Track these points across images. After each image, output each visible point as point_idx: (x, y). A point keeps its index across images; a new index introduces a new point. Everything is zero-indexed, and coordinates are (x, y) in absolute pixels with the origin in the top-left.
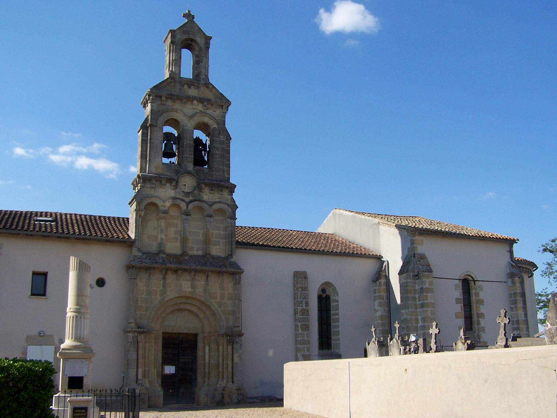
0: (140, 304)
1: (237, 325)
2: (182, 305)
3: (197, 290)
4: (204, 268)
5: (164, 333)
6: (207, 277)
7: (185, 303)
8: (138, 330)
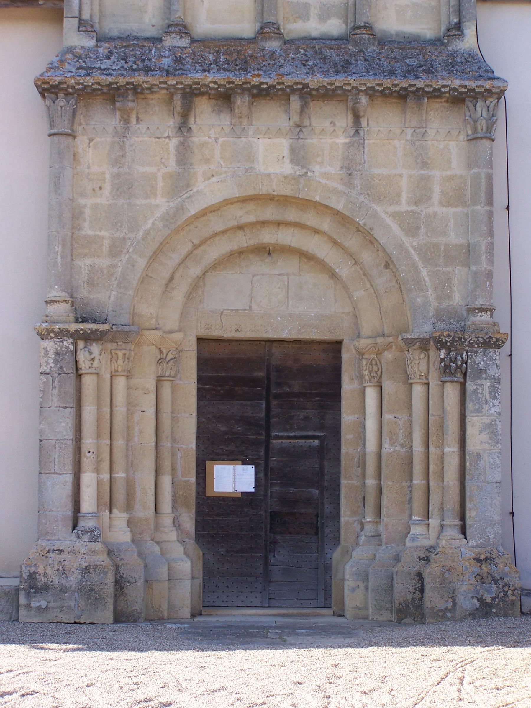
0: (90, 232)
1: (480, 302)
2: (266, 227)
3: (317, 168)
4: (339, 80)
5: (197, 336)
6: (357, 117)
7: (279, 224)
8: (73, 327)
